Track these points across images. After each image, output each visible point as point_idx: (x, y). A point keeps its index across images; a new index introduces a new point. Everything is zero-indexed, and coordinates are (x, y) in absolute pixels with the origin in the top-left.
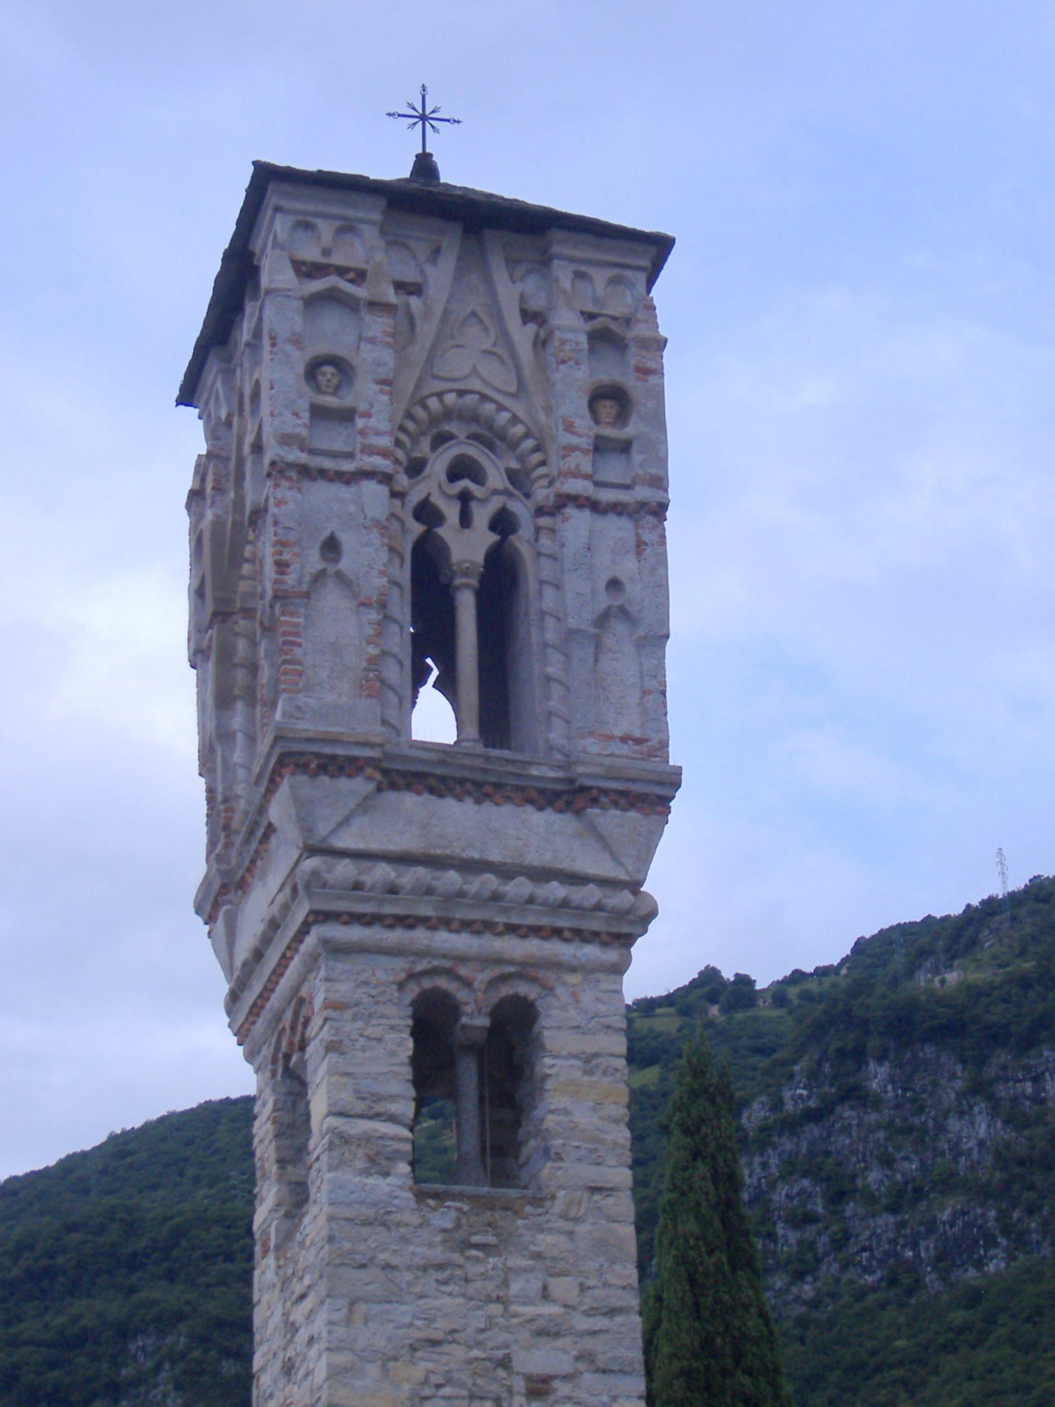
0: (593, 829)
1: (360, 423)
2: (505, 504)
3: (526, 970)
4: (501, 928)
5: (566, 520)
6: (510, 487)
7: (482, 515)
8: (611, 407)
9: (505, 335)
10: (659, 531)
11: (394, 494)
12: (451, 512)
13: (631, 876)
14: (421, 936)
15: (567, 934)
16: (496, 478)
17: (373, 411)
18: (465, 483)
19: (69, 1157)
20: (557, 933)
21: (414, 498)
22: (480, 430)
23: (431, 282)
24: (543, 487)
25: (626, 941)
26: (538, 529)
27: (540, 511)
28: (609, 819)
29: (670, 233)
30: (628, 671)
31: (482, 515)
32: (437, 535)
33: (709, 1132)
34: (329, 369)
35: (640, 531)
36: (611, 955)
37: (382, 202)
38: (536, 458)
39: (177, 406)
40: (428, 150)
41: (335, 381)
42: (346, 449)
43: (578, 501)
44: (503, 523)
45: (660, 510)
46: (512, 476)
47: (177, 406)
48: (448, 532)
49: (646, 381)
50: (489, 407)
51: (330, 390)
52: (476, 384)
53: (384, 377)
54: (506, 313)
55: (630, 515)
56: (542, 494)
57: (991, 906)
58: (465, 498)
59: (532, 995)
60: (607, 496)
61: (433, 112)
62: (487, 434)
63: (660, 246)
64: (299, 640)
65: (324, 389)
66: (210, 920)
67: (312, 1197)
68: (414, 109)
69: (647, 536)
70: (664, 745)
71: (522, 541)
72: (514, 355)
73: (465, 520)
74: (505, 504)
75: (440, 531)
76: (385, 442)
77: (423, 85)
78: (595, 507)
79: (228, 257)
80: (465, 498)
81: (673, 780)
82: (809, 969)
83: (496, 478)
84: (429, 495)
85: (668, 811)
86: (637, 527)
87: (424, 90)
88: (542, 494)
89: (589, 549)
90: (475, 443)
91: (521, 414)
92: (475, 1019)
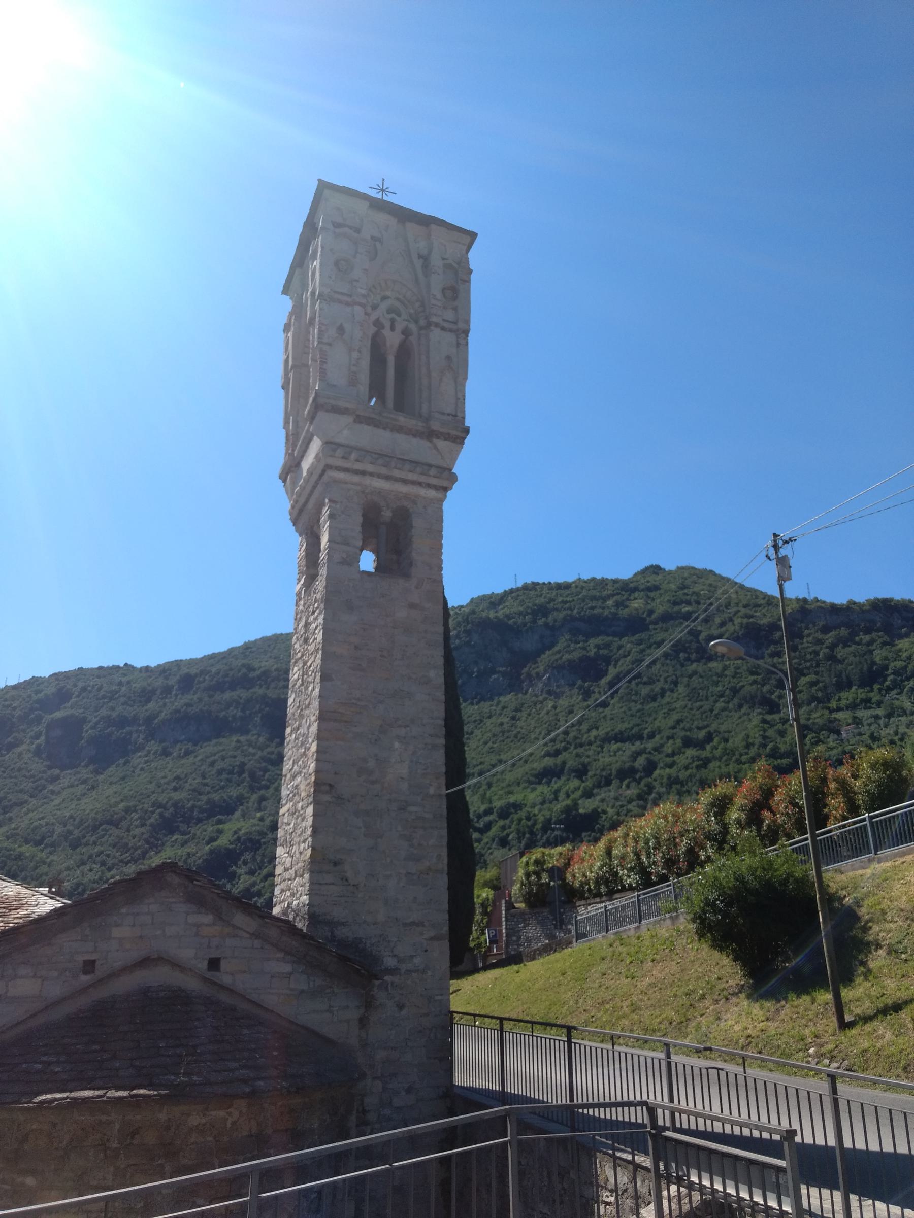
0: (436, 448)
7: (399, 327)
11: (366, 314)
12: (387, 325)
13: (311, 804)
14: (367, 481)
18: (393, 315)
19: (232, 648)
20: (420, 484)
25: (446, 489)
27: (421, 328)
28: (441, 444)
31: (399, 327)
36: (439, 495)
37: (368, 204)
44: (406, 333)
48: (386, 332)
57: (511, 591)
58: (393, 321)
59: (409, 507)
60: (446, 325)
63: (473, 236)
66: (284, 481)
67: (320, 573)
70: (464, 418)
73: (392, 328)
75: (383, 331)
78: (443, 329)
79: (306, 225)
80: (393, 321)
81: (467, 431)
82: (456, 606)
85: (463, 443)
92: (387, 514)
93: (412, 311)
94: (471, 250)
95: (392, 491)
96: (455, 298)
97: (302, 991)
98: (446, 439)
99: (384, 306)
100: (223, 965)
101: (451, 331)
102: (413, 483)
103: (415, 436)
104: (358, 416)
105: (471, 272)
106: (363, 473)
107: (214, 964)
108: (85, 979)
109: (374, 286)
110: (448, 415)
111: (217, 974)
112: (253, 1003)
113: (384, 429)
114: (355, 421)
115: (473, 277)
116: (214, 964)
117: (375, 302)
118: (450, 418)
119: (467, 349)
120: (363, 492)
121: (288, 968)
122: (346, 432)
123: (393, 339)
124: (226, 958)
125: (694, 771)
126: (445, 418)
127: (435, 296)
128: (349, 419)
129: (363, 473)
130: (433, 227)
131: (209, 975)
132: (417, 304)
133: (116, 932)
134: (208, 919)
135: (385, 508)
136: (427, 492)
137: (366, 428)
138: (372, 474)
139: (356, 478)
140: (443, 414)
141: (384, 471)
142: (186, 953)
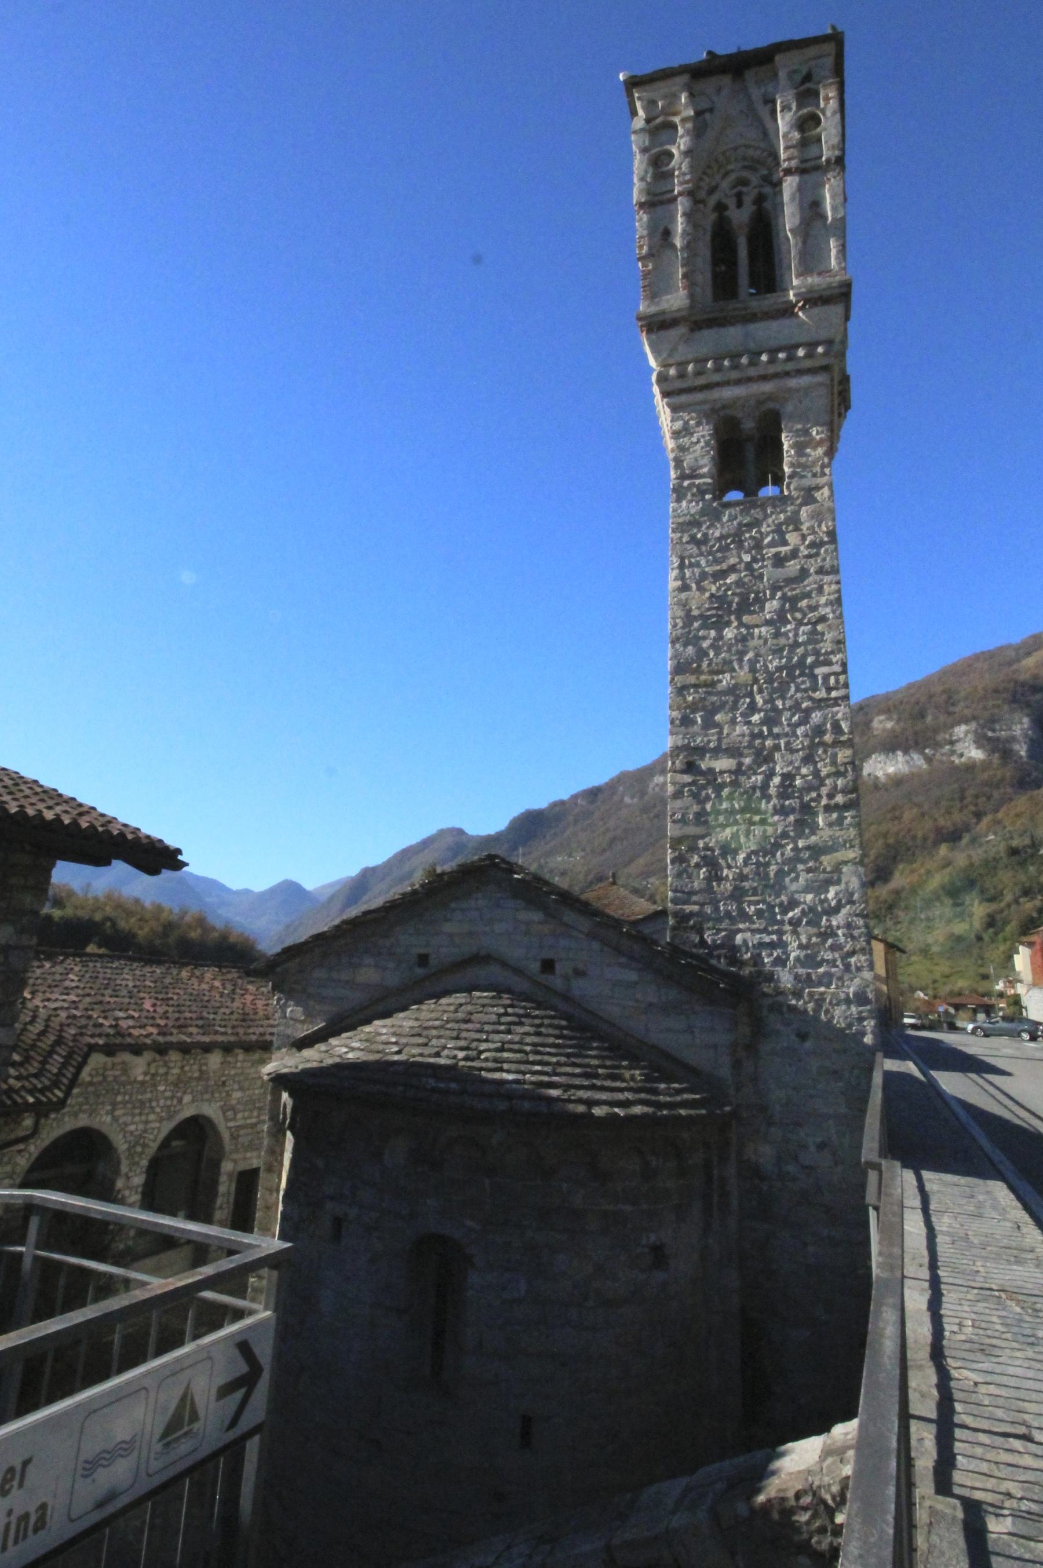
3: (770, 397)
7: (748, 200)
12: (731, 203)
14: (717, 394)
18: (740, 188)
31: (748, 200)
73: (740, 204)
75: (727, 213)
92: (749, 425)
97: (651, 1005)
100: (558, 967)
104: (696, 323)
107: (548, 966)
108: (420, 971)
109: (709, 167)
111: (550, 977)
112: (591, 1013)
114: (692, 330)
116: (548, 966)
121: (633, 976)
123: (740, 217)
124: (561, 960)
128: (681, 330)
131: (543, 978)
133: (448, 928)
134: (536, 916)
138: (718, 385)
139: (699, 396)
142: (515, 953)
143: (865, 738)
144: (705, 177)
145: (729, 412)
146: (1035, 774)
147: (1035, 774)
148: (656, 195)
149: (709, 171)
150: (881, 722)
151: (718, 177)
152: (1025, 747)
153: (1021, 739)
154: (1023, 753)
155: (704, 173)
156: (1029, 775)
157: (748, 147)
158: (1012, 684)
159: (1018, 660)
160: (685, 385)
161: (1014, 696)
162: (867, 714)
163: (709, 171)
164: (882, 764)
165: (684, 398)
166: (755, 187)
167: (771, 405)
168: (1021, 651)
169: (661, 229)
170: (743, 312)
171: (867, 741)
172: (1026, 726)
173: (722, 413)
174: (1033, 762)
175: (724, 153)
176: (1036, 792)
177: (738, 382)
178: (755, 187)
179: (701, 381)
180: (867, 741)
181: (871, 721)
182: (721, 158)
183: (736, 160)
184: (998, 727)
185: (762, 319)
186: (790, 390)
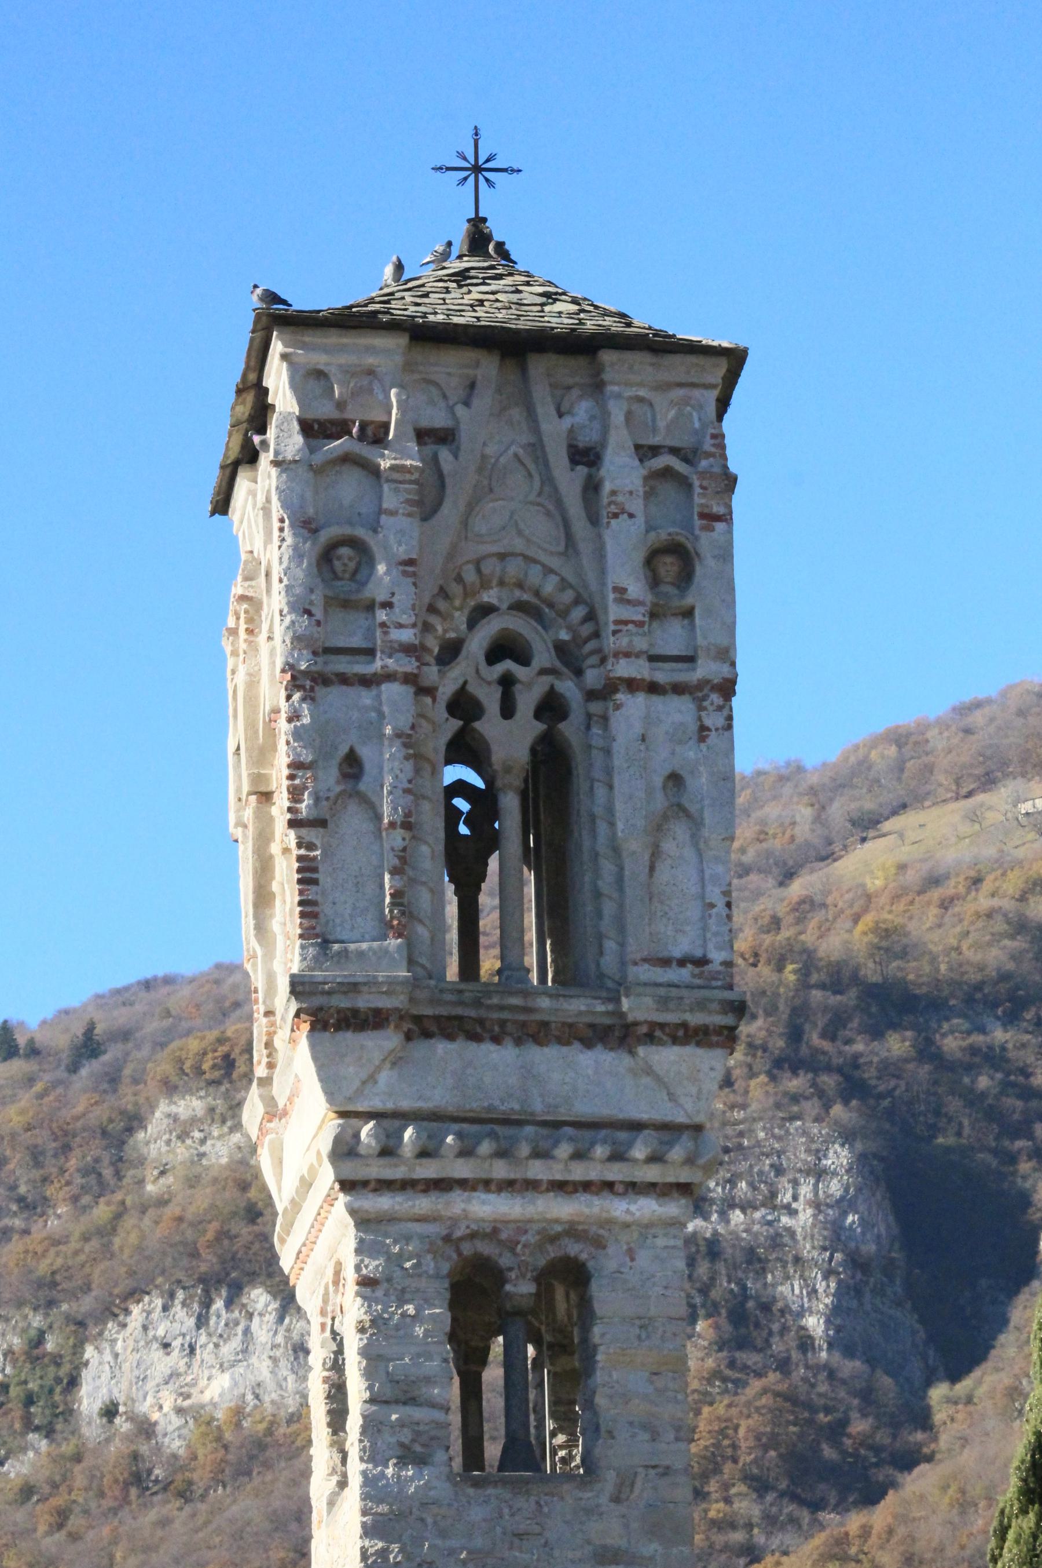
0: (649, 1071)
1: (382, 615)
2: (552, 687)
3: (573, 1231)
4: (544, 1187)
5: (618, 707)
6: (558, 664)
7: (527, 701)
8: (672, 563)
9: (548, 480)
10: (725, 712)
12: (490, 699)
15: (619, 1188)
16: (543, 656)
17: (394, 600)
18: (508, 665)
21: (447, 690)
22: (526, 597)
23: (463, 427)
24: (593, 666)
26: (589, 716)
29: (742, 344)
30: (689, 880)
31: (527, 701)
32: (474, 730)
33: (650, 1485)
34: (345, 551)
35: (703, 714)
38: (586, 630)
39: (213, 513)
40: (481, 215)
41: (352, 565)
42: (364, 645)
43: (632, 685)
45: (727, 688)
46: (561, 649)
47: (213, 513)
49: (713, 530)
50: (535, 571)
51: (347, 576)
52: (519, 545)
53: (405, 557)
54: (552, 459)
55: (691, 694)
56: (592, 677)
58: (507, 682)
59: (584, 1256)
60: (663, 675)
61: (487, 161)
62: (534, 600)
64: (315, 876)
65: (340, 575)
68: (465, 159)
69: (713, 720)
71: (570, 729)
72: (559, 503)
73: (508, 710)
74: (552, 687)
76: (407, 636)
77: (476, 127)
78: (654, 688)
80: (507, 682)
83: (543, 656)
84: (465, 683)
86: (701, 708)
87: (476, 134)
88: (592, 677)
89: (643, 740)
90: (520, 614)
91: (571, 578)
93: (564, 635)
94: (741, 381)
95: (530, 1221)
96: (686, 577)
98: (675, 1041)
99: (477, 643)
101: (679, 689)
102: (586, 1186)
103: (588, 1044)
104: (418, 1019)
105: (730, 482)
106: (441, 1185)
110: (682, 963)
113: (497, 1040)
114: (409, 1037)
115: (739, 500)
117: (452, 635)
118: (685, 974)
119: (731, 741)
120: (447, 1239)
122: (385, 1077)
125: (972, 928)
126: (673, 974)
127: (623, 591)
129: (441, 1185)
130: (607, 357)
132: (578, 613)
135: (513, 1275)
136: (633, 1208)
137: (441, 1047)
138: (463, 1184)
139: (423, 1204)
140: (665, 962)
141: (500, 1170)
143: (102, 1212)
144: (433, 620)
145: (485, 1248)
146: (859, 1426)
147: (859, 1426)
148: (328, 651)
149: (442, 605)
150: (182, 1130)
151: (461, 619)
152: (826, 1292)
153: (807, 1250)
154: (815, 1324)
155: (432, 609)
156: (837, 1430)
157: (529, 560)
158: (790, 974)
159: (827, 857)
160: (398, 1173)
161: (795, 1035)
162: (113, 1079)
163: (442, 605)
164: (176, 1359)
165: (384, 1203)
166: (543, 672)
167: (573, 1248)
168: (839, 810)
169: (344, 750)
170: (522, 1017)
171: (108, 1231)
172: (835, 1187)
173: (467, 1249)
174: (850, 1367)
175: (478, 563)
176: (855, 1521)
177: (508, 1185)
178: (543, 672)
179: (428, 1170)
180: (108, 1231)
181: (134, 1121)
182: (470, 576)
183: (501, 583)
184: (715, 1188)
185: (563, 1041)
186: (609, 1223)
